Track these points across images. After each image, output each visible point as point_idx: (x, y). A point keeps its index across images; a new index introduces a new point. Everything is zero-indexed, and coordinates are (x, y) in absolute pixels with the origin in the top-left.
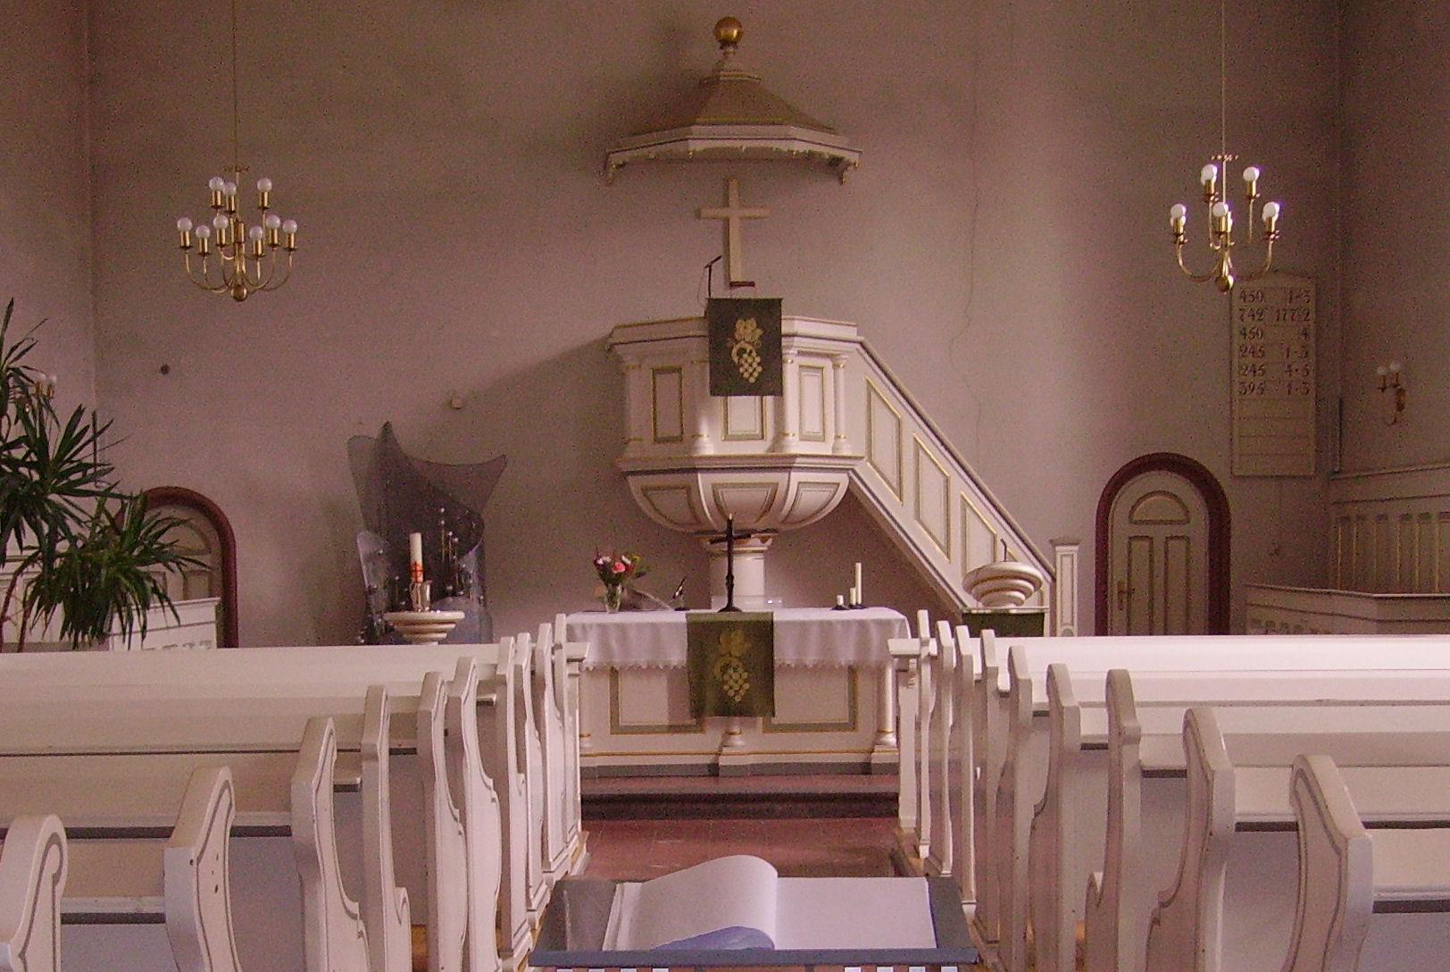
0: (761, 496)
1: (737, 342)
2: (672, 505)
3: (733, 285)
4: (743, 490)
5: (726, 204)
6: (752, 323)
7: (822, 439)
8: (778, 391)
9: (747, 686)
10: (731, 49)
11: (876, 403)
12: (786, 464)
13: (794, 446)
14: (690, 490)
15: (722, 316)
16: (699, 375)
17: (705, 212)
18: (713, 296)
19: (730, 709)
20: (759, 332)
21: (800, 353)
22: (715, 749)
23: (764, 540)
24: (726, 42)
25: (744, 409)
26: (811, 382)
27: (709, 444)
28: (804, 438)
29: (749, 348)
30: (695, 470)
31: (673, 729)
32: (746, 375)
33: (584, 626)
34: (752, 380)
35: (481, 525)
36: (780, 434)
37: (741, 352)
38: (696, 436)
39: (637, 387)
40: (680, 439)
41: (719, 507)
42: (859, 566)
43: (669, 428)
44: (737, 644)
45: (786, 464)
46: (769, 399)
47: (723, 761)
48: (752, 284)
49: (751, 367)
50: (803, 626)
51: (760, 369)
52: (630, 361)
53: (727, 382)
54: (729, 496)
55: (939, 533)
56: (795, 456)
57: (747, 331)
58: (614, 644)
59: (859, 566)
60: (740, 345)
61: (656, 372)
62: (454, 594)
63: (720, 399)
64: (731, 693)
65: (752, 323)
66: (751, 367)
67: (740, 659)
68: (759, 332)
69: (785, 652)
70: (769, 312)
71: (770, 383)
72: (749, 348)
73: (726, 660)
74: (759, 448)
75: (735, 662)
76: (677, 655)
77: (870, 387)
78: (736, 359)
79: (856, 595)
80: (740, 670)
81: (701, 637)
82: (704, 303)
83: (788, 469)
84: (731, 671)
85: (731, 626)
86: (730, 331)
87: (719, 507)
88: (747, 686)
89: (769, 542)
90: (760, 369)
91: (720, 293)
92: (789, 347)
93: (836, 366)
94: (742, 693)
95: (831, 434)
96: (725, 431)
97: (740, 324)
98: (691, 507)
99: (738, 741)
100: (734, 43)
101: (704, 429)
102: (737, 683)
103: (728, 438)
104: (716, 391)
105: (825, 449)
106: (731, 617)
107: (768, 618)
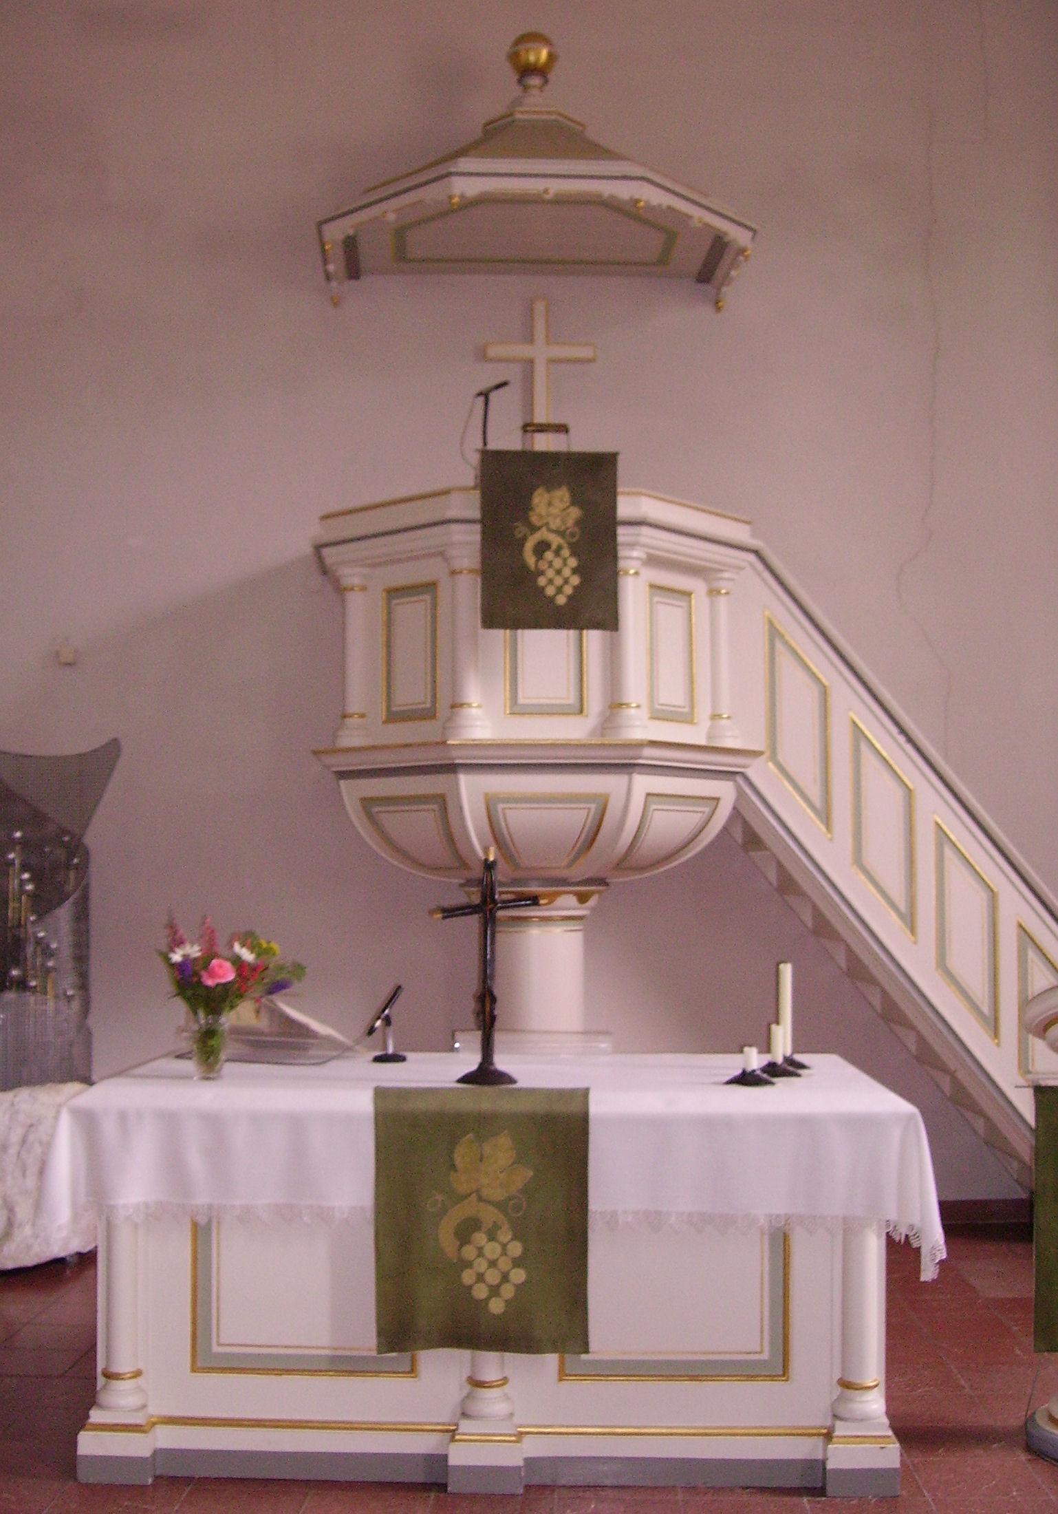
0: (575, 819)
1: (534, 529)
2: (416, 828)
3: (530, 428)
4: (540, 809)
5: (530, 339)
6: (562, 495)
7: (687, 718)
8: (608, 620)
9: (519, 1276)
10: (535, 81)
11: (785, 661)
12: (625, 762)
13: (639, 726)
14: (443, 805)
15: (508, 483)
16: (466, 595)
17: (493, 352)
18: (492, 446)
19: (469, 1331)
20: (575, 513)
21: (653, 561)
22: (444, 1415)
23: (583, 898)
24: (526, 71)
25: (546, 652)
26: (670, 615)
27: (482, 721)
28: (659, 715)
29: (556, 541)
30: (452, 768)
31: (343, 1365)
32: (550, 591)
33: (123, 1117)
34: (561, 600)
35: (86, 855)
36: (615, 705)
37: (542, 548)
38: (457, 706)
39: (362, 613)
40: (428, 714)
41: (497, 836)
42: (787, 971)
43: (411, 694)
44: (496, 1171)
45: (625, 762)
46: (593, 637)
47: (458, 1456)
48: (562, 429)
49: (559, 576)
50: (661, 1127)
51: (575, 580)
52: (351, 576)
53: (512, 601)
54: (517, 820)
55: (895, 886)
56: (641, 745)
57: (553, 510)
58: (196, 1161)
59: (787, 971)
60: (543, 535)
61: (394, 593)
62: (22, 985)
63: (499, 636)
64: (480, 1292)
65: (562, 495)
66: (559, 576)
67: (500, 1206)
68: (575, 513)
69: (615, 1184)
70: (593, 476)
71: (594, 607)
72: (556, 541)
73: (457, 1214)
74: (574, 730)
75: (490, 1215)
76: (351, 1186)
77: (774, 633)
78: (530, 560)
79: (783, 1042)
80: (505, 1235)
81: (411, 1144)
82: (475, 459)
83: (627, 768)
84: (480, 1238)
85: (484, 1124)
86: (522, 507)
87: (497, 836)
88: (519, 1276)
89: (592, 902)
90: (575, 580)
91: (507, 439)
92: (632, 545)
93: (713, 593)
94: (508, 1291)
95: (703, 712)
96: (512, 693)
97: (540, 499)
98: (450, 838)
99: (493, 1403)
100: (541, 71)
101: (473, 693)
102: (495, 1268)
103: (517, 709)
104: (491, 619)
105: (695, 735)
106: (485, 1099)
107: (574, 1107)
